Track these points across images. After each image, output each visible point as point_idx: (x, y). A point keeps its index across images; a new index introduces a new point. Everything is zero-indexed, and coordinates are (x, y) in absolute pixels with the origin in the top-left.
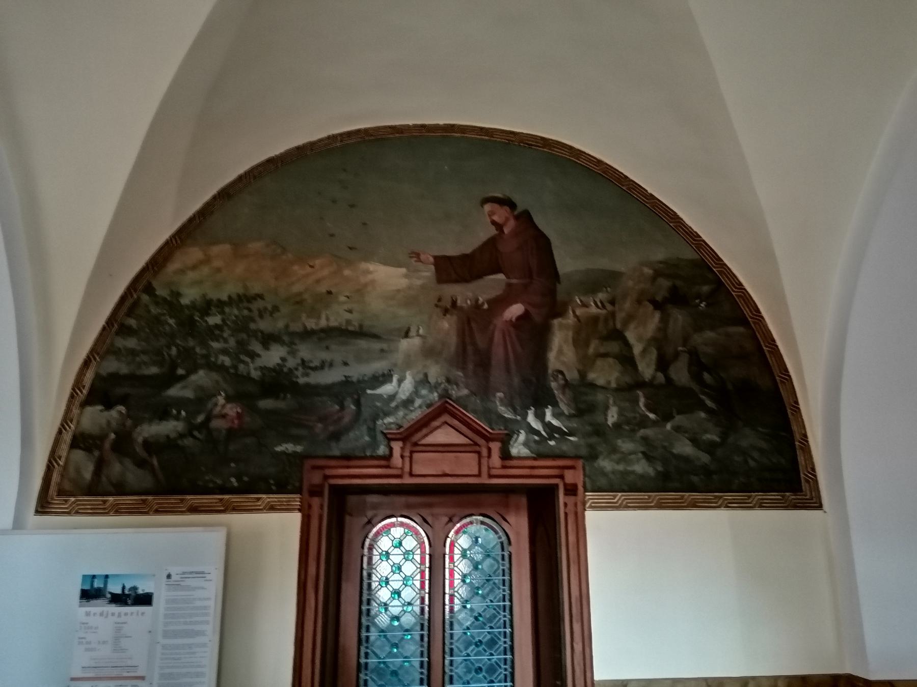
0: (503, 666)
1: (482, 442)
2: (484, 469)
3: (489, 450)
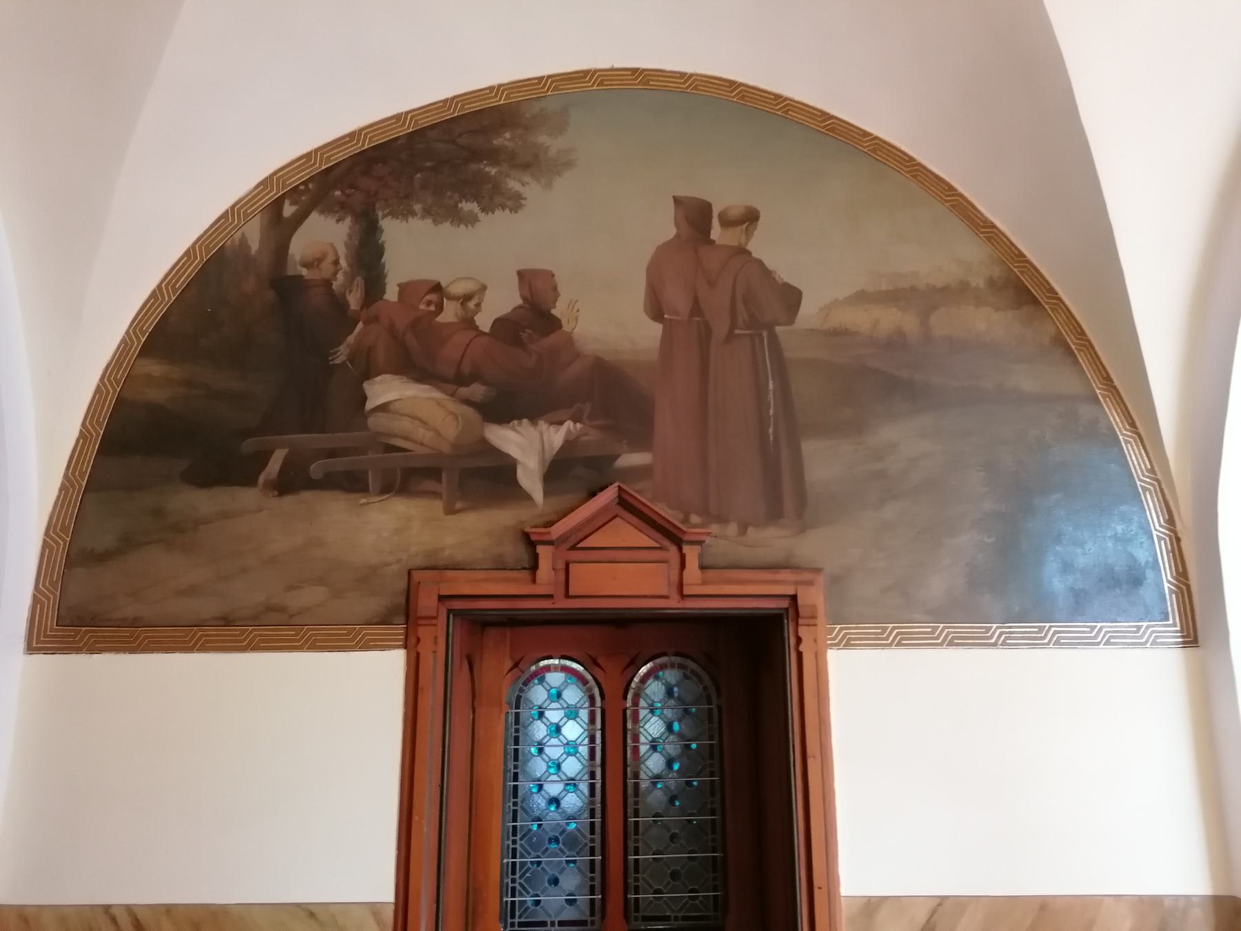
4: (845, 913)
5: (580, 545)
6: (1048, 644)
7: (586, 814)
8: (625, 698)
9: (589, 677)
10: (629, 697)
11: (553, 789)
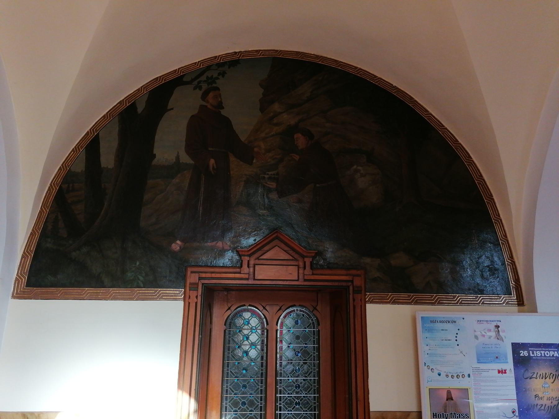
0: (313, 385)
1: (300, 259)
2: (301, 277)
3: (305, 263)
4: (372, 415)
5: (261, 258)
6: (457, 303)
7: (259, 359)
8: (277, 325)
10: (279, 324)
11: (246, 348)
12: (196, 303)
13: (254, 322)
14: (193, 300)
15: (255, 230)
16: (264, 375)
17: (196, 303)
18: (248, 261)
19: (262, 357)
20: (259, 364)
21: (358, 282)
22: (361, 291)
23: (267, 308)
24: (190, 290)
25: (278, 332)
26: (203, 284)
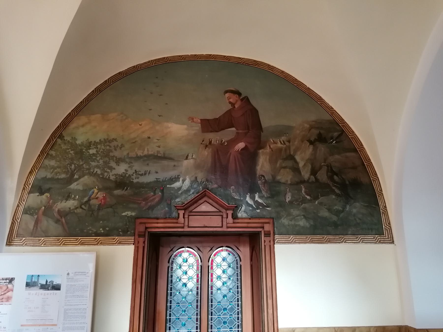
1: (223, 210)
2: (225, 223)
3: (227, 214)
8: (209, 262)
9: (196, 254)
11: (184, 268)
12: (144, 247)
13: (192, 260)
14: (141, 245)
15: (142, 186)
16: (199, 301)
17: (144, 247)
18: (184, 214)
19: (197, 288)
20: (195, 292)
21: (267, 227)
22: (270, 234)
23: (201, 249)
24: (264, 236)
25: (210, 267)
26: (261, 231)
